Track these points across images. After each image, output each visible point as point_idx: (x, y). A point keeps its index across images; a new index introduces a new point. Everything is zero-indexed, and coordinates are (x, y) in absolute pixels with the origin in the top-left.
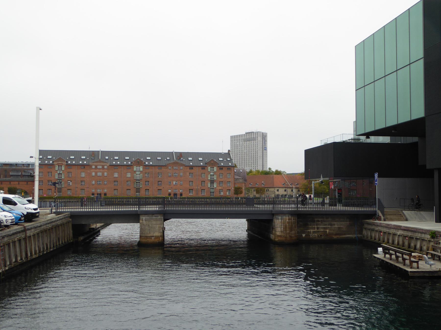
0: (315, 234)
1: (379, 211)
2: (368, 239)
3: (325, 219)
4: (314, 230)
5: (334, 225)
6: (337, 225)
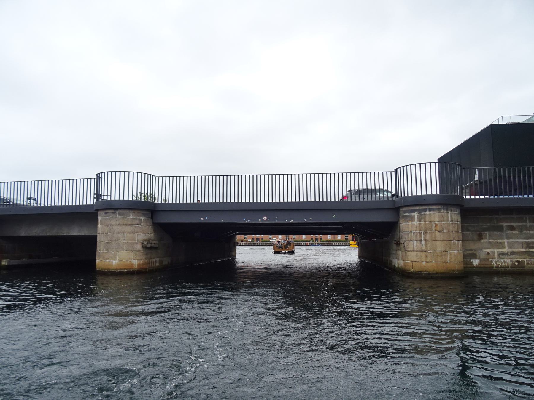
0: (506, 260)
2: (525, 270)
3: (528, 224)
4: (501, 250)
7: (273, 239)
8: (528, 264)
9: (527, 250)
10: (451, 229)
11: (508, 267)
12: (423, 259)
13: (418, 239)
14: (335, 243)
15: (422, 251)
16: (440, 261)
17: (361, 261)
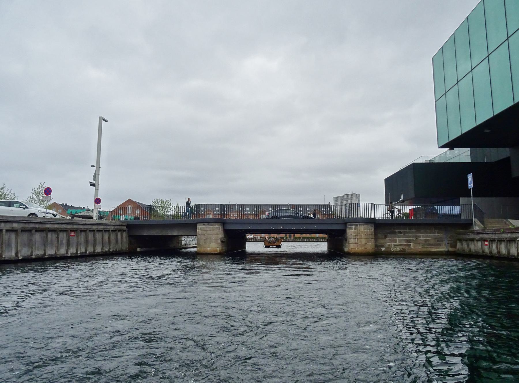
0: (397, 248)
1: (476, 219)
3: (408, 231)
4: (395, 243)
5: (420, 237)
6: (423, 238)
7: (250, 236)
8: (407, 250)
9: (407, 243)
10: (369, 234)
11: (398, 252)
12: (356, 247)
13: (354, 238)
14: (306, 240)
15: (356, 243)
16: (363, 248)
17: (328, 251)
